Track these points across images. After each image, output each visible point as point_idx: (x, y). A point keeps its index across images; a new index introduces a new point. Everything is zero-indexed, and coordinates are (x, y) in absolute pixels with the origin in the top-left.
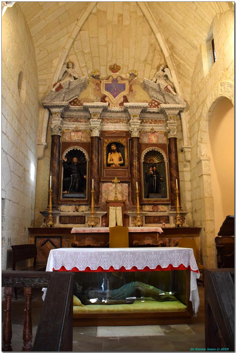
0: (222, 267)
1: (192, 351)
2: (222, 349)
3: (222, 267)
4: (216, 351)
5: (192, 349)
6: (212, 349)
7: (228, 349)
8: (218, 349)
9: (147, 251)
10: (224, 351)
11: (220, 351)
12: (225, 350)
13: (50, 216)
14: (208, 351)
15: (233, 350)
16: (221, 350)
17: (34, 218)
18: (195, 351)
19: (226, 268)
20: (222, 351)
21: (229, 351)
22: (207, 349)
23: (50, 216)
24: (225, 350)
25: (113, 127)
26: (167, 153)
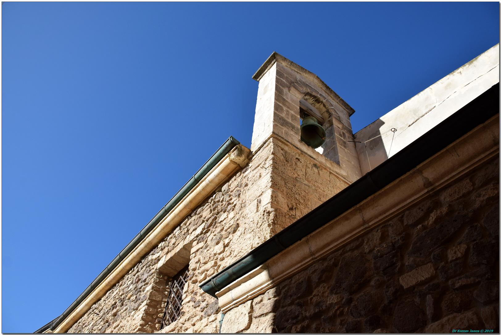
0: (278, 77)
1: (454, 333)
2: (486, 331)
3: (278, 77)
4: (480, 333)
5: (454, 331)
6: (475, 331)
7: (492, 331)
8: (481, 331)
9: (261, 76)
10: (488, 333)
11: (484, 333)
12: (489, 331)
13: (363, 313)
14: (471, 333)
15: (498, 332)
16: (485, 332)
17: (319, 135)
18: (456, 333)
19: (383, 115)
20: (486, 333)
21: (494, 332)
22: (469, 331)
23: (363, 313)
24: (489, 331)
25: (180, 247)
26: (171, 332)
